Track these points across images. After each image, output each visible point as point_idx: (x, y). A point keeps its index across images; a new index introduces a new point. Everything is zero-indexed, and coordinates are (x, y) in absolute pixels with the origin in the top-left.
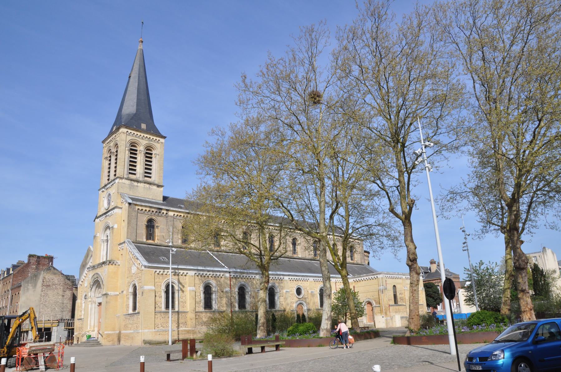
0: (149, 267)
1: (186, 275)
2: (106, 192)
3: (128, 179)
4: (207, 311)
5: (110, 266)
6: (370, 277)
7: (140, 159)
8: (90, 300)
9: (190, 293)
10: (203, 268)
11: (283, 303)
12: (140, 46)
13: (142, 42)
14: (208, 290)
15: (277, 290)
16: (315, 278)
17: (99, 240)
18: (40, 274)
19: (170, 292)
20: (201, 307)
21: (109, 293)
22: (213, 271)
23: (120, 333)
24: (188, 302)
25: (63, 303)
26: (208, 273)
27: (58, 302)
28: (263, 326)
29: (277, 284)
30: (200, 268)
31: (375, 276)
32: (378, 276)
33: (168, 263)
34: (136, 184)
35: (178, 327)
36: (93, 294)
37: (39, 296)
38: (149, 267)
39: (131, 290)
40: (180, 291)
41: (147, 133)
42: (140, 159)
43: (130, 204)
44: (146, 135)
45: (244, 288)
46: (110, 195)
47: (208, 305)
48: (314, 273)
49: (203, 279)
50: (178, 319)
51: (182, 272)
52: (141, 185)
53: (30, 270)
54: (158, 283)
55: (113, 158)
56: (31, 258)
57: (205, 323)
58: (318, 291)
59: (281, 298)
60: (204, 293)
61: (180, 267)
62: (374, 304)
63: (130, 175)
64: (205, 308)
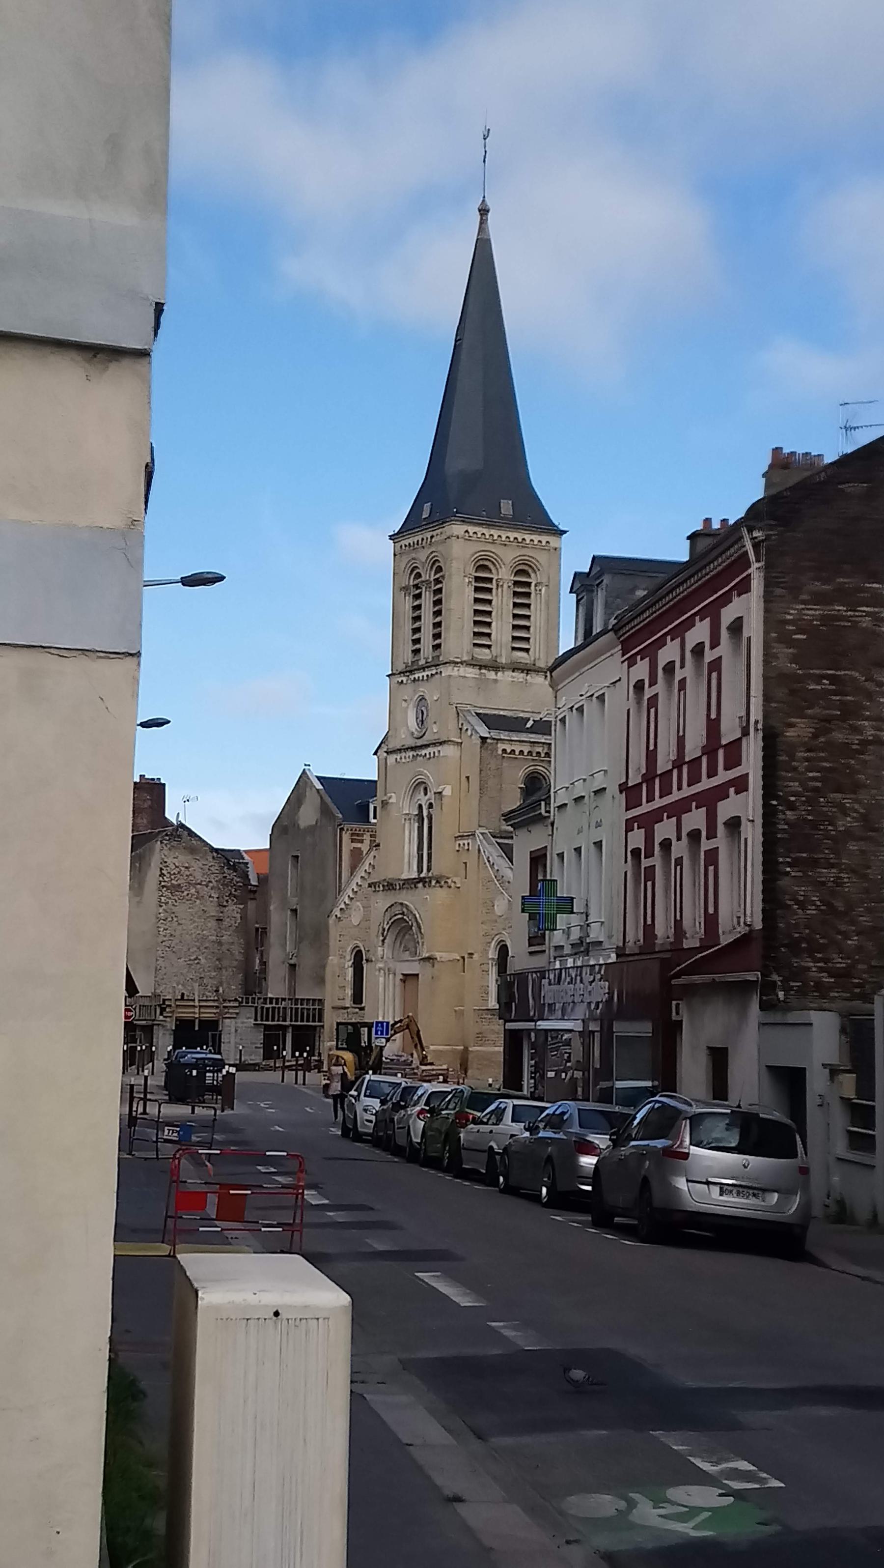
2: (410, 688)
3: (473, 663)
7: (502, 602)
8: (381, 965)
17: (394, 813)
18: (152, 850)
21: (438, 955)
23: (466, 1049)
25: (220, 943)
27: (205, 938)
34: (491, 675)
36: (388, 953)
37: (154, 920)
39: (493, 954)
41: (515, 528)
42: (502, 602)
43: (484, 739)
46: (422, 698)
52: (506, 677)
55: (427, 600)
63: (477, 650)
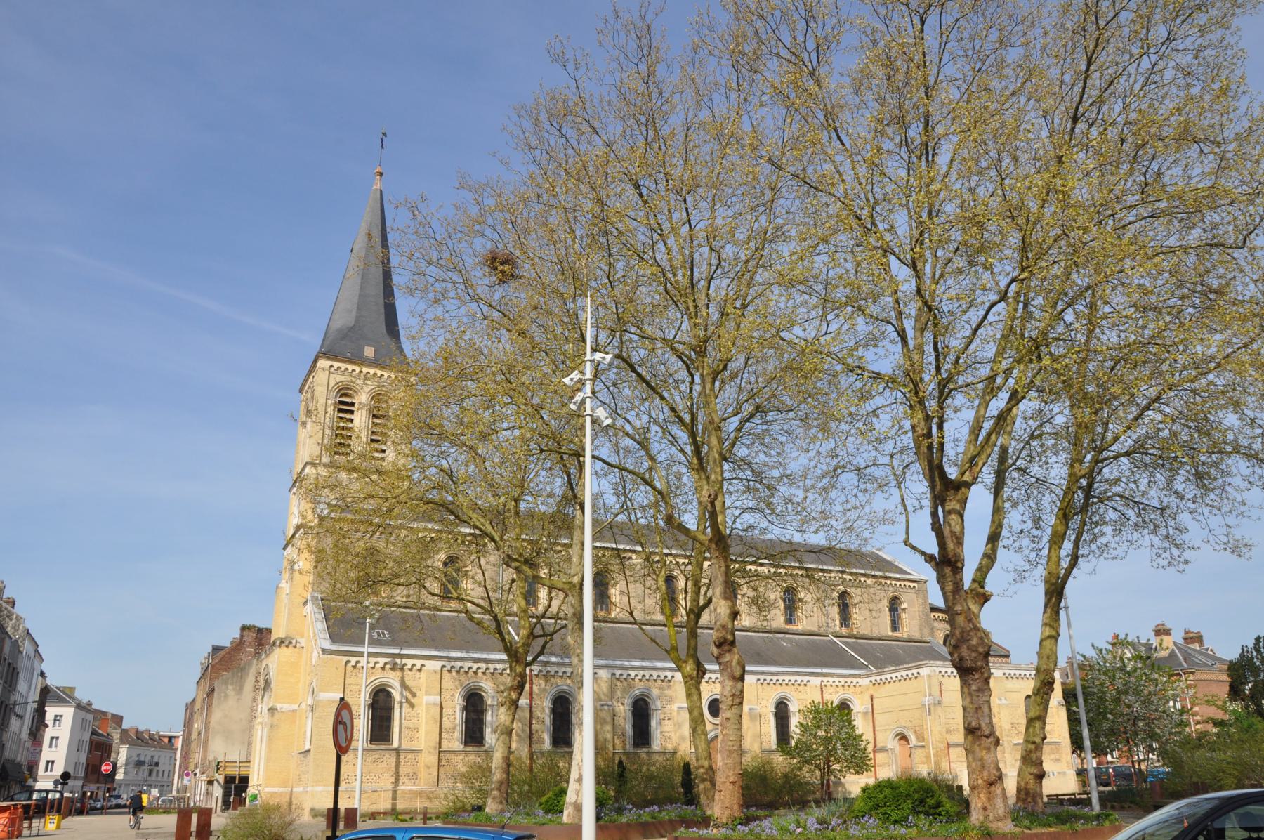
0: (332, 652)
1: (420, 670)
4: (374, 747)
5: (283, 649)
6: (904, 674)
9: (427, 709)
10: (464, 655)
11: (672, 734)
12: (378, 184)
13: (381, 174)
14: (474, 704)
15: (656, 705)
16: (762, 677)
19: (381, 704)
20: (454, 741)
21: (279, 706)
22: (487, 661)
24: (423, 729)
26: (475, 666)
28: (499, 789)
29: (655, 692)
30: (453, 654)
31: (915, 672)
32: (920, 670)
33: (362, 643)
35: (397, 782)
38: (332, 652)
40: (405, 705)
44: (372, 371)
45: (567, 699)
47: (474, 734)
48: (767, 663)
49: (463, 678)
50: (397, 766)
51: (409, 662)
53: (243, 657)
54: (352, 688)
56: (246, 633)
57: (462, 775)
58: (772, 708)
59: (666, 722)
60: (466, 708)
61: (405, 652)
62: (912, 738)
64: (466, 744)
